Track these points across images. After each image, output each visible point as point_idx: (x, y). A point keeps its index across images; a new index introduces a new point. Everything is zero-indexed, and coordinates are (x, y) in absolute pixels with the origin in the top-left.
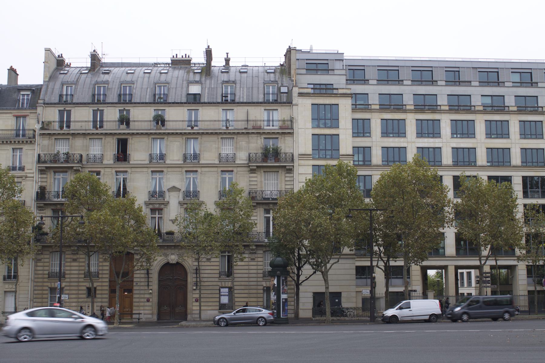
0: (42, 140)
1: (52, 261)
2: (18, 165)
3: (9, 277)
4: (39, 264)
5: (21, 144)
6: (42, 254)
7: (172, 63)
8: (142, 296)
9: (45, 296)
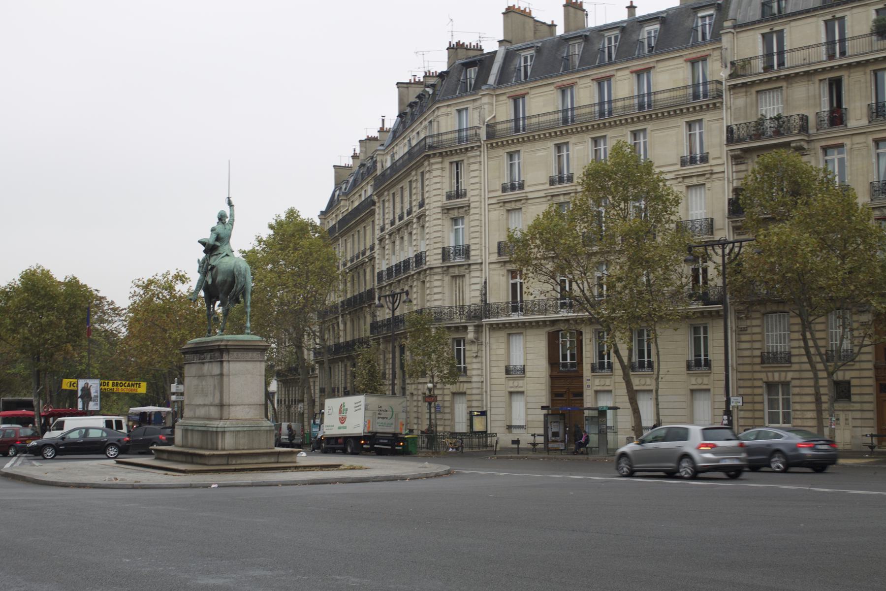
0: (734, 99)
1: (768, 331)
2: (698, 152)
3: (698, 363)
5: (699, 111)
6: (747, 318)
9: (757, 399)
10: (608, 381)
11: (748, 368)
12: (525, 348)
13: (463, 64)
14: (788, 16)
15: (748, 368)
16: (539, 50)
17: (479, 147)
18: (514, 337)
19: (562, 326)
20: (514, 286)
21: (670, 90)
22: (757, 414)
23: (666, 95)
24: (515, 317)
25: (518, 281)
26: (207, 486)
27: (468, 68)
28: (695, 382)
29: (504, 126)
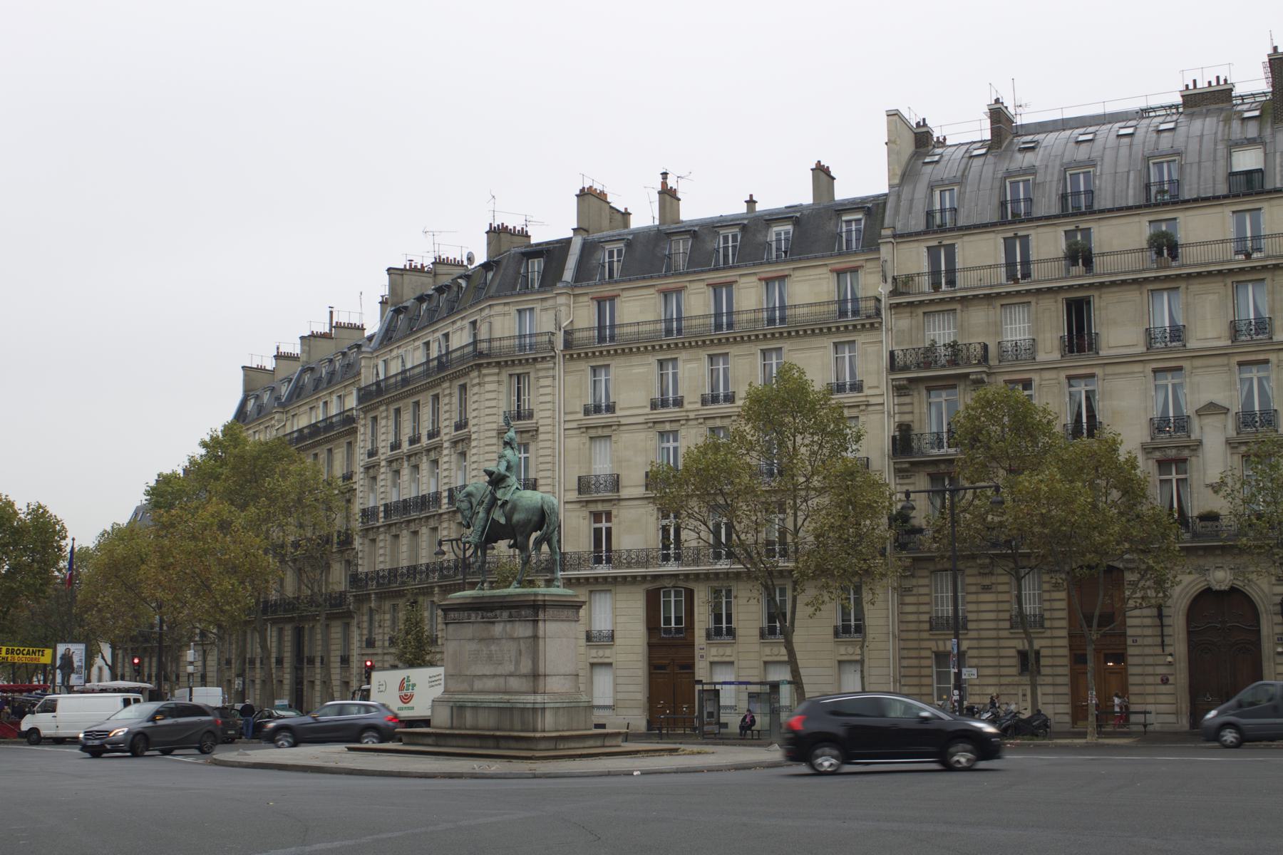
1: (936, 592)
2: (721, 390)
4: (908, 599)
7: (1185, 104)
8: (1150, 670)
10: (728, 651)
11: (914, 635)
12: (614, 609)
13: (524, 254)
14: (961, 229)
15: (914, 635)
16: (629, 244)
17: (553, 357)
18: (598, 596)
19: (668, 583)
20: (597, 532)
21: (811, 305)
22: (925, 690)
23: (805, 310)
24: (602, 570)
25: (604, 525)
26: (630, 774)
27: (517, 263)
28: (848, 651)
29: (585, 334)
